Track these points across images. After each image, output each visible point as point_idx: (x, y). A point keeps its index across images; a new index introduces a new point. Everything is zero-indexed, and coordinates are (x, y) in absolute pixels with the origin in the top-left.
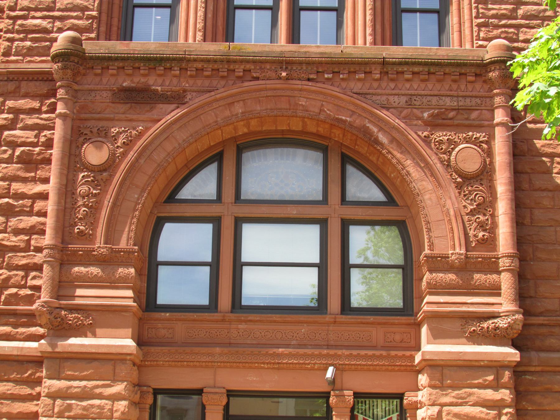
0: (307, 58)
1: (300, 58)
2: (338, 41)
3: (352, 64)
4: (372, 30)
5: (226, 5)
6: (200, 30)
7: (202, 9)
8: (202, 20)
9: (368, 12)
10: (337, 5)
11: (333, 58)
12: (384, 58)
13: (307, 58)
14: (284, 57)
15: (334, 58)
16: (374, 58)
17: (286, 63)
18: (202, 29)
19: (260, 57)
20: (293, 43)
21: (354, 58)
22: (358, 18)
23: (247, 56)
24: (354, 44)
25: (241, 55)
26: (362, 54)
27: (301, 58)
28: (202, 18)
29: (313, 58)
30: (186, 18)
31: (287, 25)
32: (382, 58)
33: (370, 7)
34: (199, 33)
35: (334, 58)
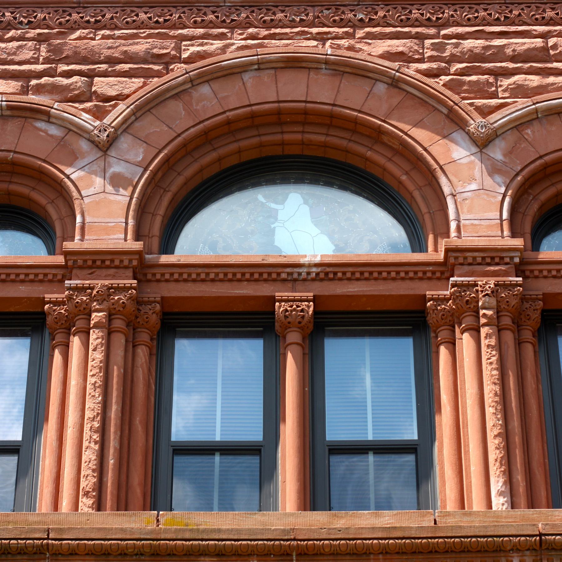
0: (350, 539)
1: (333, 540)
2: (463, 220)
3: (463, 551)
4: (505, 483)
5: (151, 441)
6: (86, 494)
7: (92, 445)
8: (94, 471)
9: (493, 443)
10: (415, 436)
11: (415, 538)
12: (540, 535)
13: (350, 539)
14: (294, 539)
15: (419, 538)
16: (517, 536)
17: (297, 555)
18: (94, 490)
19: (235, 540)
20: (314, 508)
21: (467, 537)
22: (468, 460)
23: (202, 540)
24: (463, 507)
25: (187, 536)
26: (485, 527)
27: (337, 540)
28: (93, 465)
29: (366, 539)
30: (54, 470)
31: (299, 480)
32: (536, 535)
33: (496, 431)
34: (85, 500)
35: (419, 538)
